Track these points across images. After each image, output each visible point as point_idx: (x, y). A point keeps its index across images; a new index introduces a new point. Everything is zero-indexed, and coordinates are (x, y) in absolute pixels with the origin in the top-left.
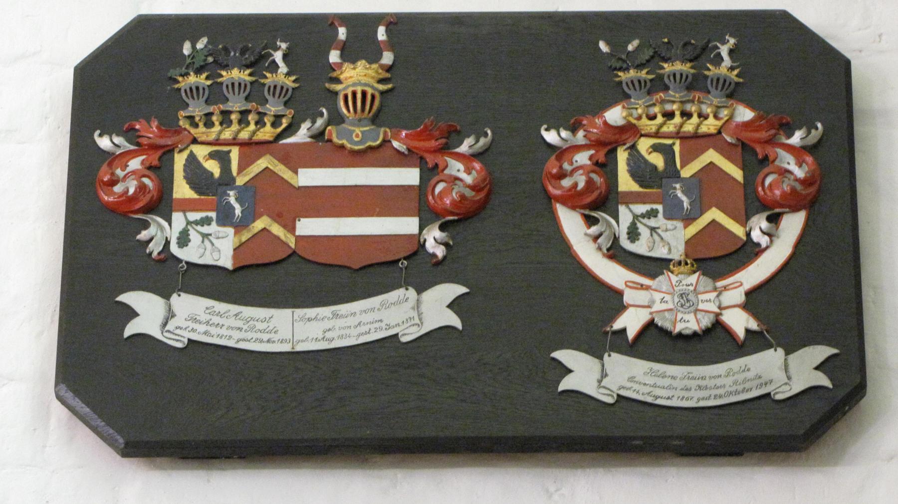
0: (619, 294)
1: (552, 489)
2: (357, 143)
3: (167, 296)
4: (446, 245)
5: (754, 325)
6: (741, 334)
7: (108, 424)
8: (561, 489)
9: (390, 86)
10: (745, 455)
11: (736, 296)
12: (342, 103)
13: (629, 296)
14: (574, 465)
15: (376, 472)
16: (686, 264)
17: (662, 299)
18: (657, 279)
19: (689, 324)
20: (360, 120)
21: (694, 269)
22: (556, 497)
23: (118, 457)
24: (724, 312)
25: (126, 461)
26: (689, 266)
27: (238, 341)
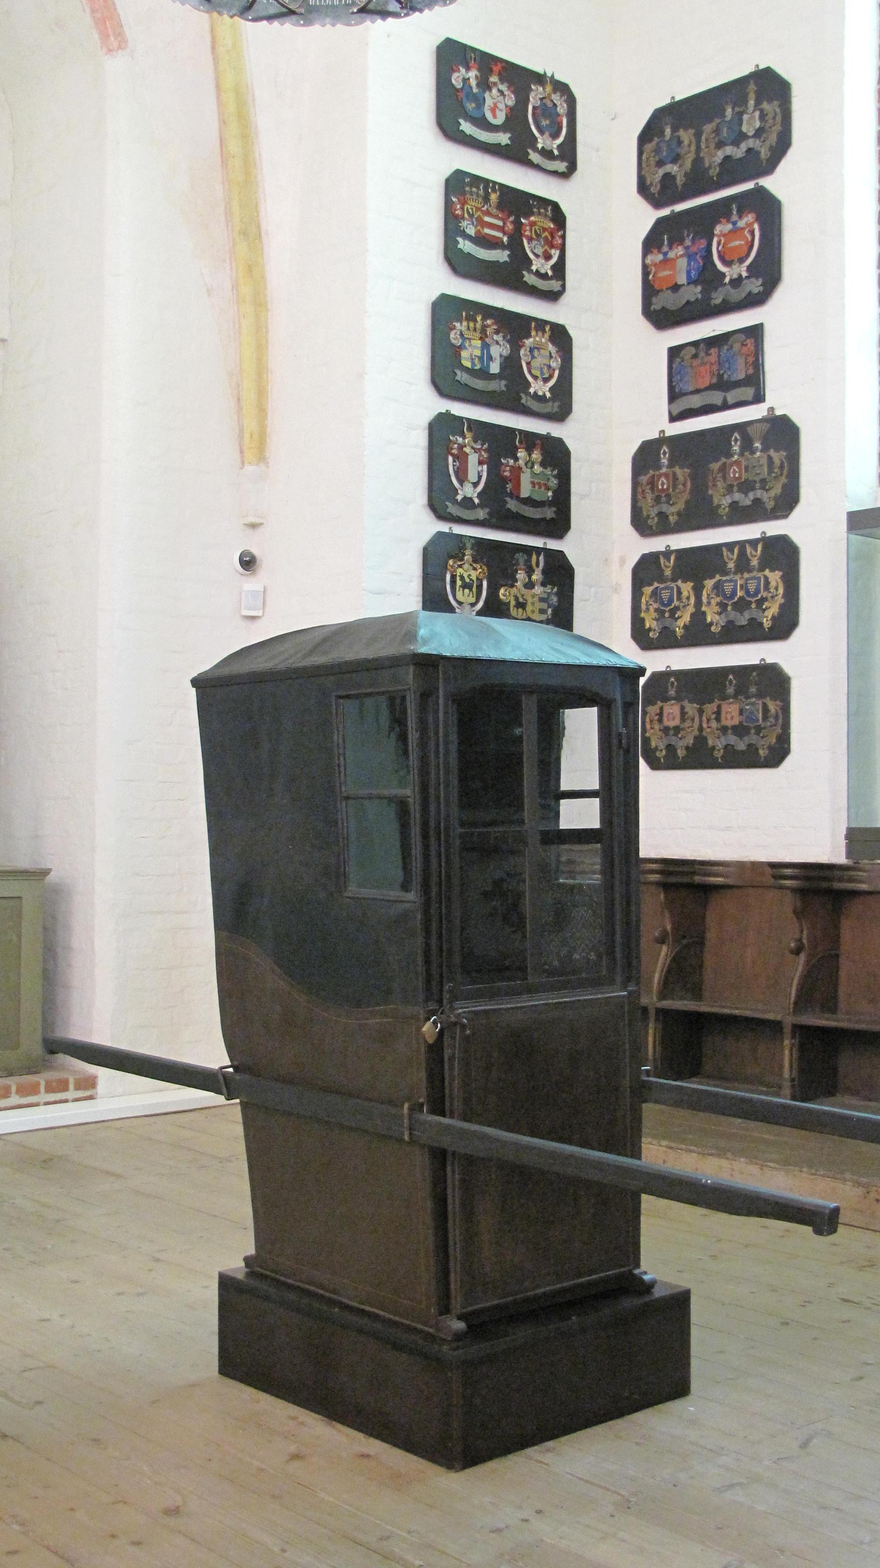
11: (476, 495)
13: (532, 385)
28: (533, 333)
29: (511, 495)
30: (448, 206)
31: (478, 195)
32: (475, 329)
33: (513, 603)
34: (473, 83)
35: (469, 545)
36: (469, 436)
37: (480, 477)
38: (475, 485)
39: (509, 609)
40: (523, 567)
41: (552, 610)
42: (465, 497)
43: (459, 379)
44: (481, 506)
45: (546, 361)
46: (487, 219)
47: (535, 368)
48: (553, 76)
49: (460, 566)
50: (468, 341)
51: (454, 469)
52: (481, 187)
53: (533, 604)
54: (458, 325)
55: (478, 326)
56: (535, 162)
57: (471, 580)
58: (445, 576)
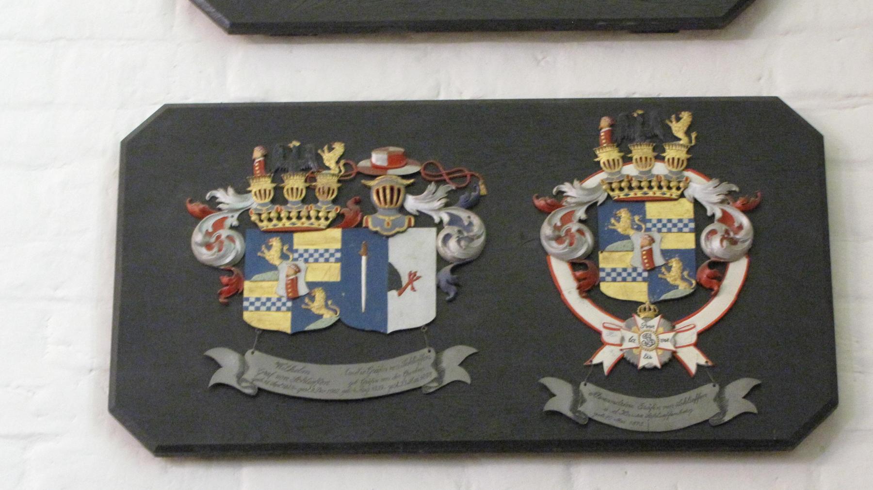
0: (599, 333)
1: (540, 57)
2: (387, 230)
3: (243, 353)
4: (457, 285)
5: (702, 360)
6: (693, 369)
7: (218, 10)
8: (546, 57)
9: (412, 181)
10: (680, 32)
11: (692, 337)
12: (375, 198)
13: (606, 336)
14: (556, 41)
15: (413, 46)
16: (650, 309)
17: (630, 339)
18: (627, 321)
19: (650, 359)
20: (389, 209)
21: (656, 313)
22: (542, 63)
23: (225, 35)
24: (679, 350)
25: (231, 37)
26: (652, 311)
27: (298, 392)
28: (606, 154)
42: (581, 181)
54: (227, 197)
55: (327, 181)
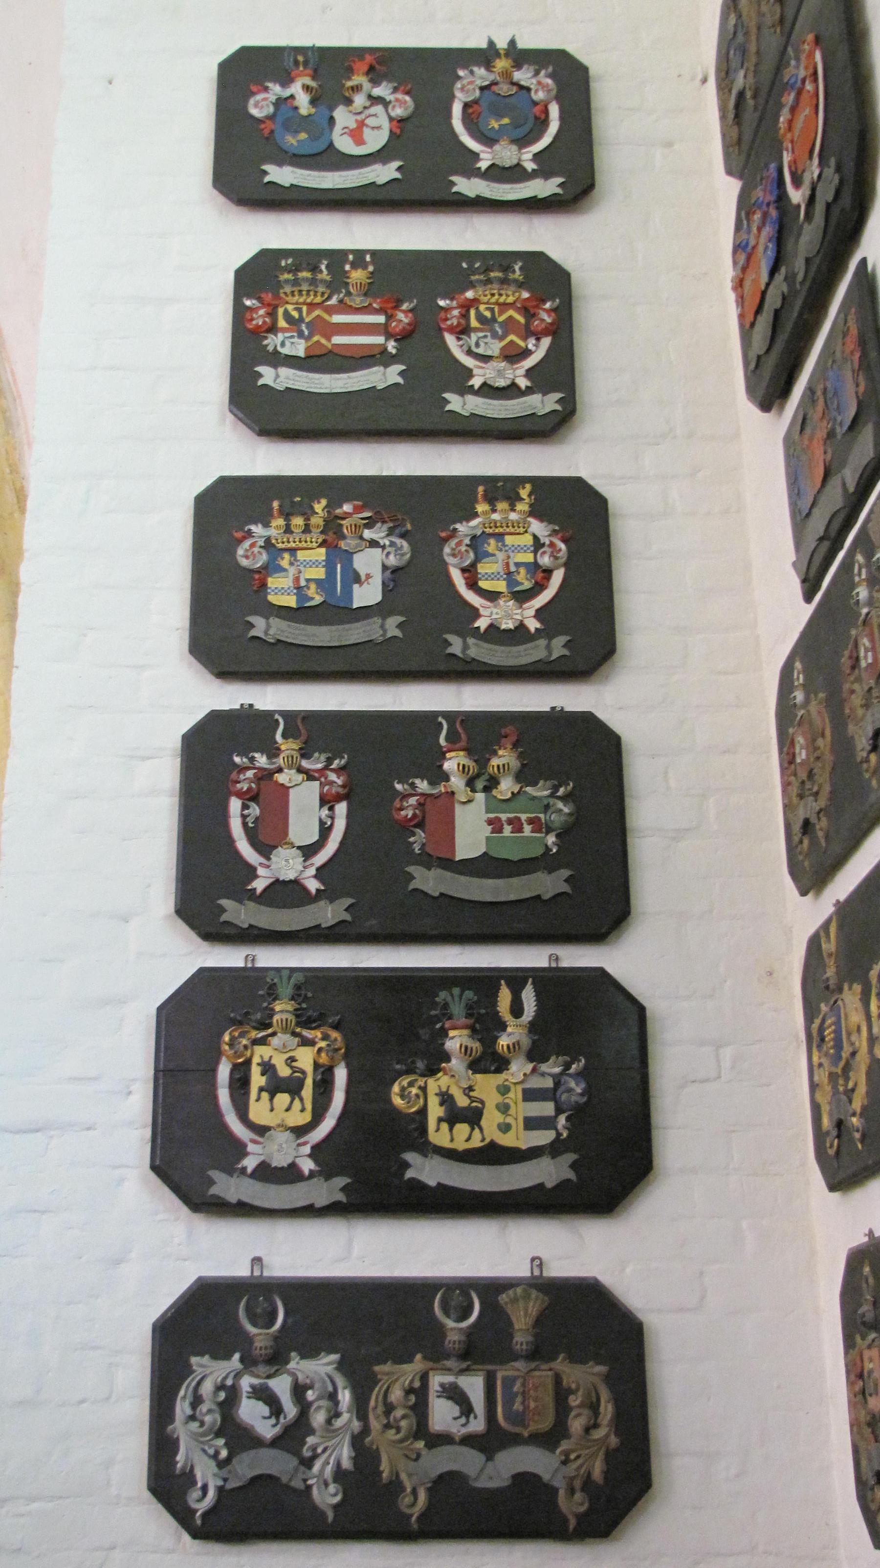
11: (312, 871)
28: (481, 508)
29: (427, 860)
30: (240, 314)
31: (313, 282)
32: (307, 529)
33: (435, 1111)
34: (303, 101)
35: (285, 990)
36: (288, 747)
37: (325, 831)
38: (309, 851)
39: (423, 1130)
40: (463, 1021)
41: (568, 1119)
43: (261, 634)
44: (327, 894)
45: (529, 558)
46: (338, 319)
47: (489, 577)
48: (512, 43)
49: (262, 1042)
50: (287, 556)
51: (245, 824)
52: (323, 267)
53: (504, 1109)
54: (257, 529)
55: (317, 521)
56: (472, 194)
57: (295, 1070)
58: (214, 1071)
